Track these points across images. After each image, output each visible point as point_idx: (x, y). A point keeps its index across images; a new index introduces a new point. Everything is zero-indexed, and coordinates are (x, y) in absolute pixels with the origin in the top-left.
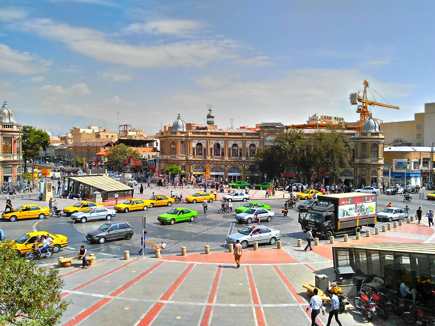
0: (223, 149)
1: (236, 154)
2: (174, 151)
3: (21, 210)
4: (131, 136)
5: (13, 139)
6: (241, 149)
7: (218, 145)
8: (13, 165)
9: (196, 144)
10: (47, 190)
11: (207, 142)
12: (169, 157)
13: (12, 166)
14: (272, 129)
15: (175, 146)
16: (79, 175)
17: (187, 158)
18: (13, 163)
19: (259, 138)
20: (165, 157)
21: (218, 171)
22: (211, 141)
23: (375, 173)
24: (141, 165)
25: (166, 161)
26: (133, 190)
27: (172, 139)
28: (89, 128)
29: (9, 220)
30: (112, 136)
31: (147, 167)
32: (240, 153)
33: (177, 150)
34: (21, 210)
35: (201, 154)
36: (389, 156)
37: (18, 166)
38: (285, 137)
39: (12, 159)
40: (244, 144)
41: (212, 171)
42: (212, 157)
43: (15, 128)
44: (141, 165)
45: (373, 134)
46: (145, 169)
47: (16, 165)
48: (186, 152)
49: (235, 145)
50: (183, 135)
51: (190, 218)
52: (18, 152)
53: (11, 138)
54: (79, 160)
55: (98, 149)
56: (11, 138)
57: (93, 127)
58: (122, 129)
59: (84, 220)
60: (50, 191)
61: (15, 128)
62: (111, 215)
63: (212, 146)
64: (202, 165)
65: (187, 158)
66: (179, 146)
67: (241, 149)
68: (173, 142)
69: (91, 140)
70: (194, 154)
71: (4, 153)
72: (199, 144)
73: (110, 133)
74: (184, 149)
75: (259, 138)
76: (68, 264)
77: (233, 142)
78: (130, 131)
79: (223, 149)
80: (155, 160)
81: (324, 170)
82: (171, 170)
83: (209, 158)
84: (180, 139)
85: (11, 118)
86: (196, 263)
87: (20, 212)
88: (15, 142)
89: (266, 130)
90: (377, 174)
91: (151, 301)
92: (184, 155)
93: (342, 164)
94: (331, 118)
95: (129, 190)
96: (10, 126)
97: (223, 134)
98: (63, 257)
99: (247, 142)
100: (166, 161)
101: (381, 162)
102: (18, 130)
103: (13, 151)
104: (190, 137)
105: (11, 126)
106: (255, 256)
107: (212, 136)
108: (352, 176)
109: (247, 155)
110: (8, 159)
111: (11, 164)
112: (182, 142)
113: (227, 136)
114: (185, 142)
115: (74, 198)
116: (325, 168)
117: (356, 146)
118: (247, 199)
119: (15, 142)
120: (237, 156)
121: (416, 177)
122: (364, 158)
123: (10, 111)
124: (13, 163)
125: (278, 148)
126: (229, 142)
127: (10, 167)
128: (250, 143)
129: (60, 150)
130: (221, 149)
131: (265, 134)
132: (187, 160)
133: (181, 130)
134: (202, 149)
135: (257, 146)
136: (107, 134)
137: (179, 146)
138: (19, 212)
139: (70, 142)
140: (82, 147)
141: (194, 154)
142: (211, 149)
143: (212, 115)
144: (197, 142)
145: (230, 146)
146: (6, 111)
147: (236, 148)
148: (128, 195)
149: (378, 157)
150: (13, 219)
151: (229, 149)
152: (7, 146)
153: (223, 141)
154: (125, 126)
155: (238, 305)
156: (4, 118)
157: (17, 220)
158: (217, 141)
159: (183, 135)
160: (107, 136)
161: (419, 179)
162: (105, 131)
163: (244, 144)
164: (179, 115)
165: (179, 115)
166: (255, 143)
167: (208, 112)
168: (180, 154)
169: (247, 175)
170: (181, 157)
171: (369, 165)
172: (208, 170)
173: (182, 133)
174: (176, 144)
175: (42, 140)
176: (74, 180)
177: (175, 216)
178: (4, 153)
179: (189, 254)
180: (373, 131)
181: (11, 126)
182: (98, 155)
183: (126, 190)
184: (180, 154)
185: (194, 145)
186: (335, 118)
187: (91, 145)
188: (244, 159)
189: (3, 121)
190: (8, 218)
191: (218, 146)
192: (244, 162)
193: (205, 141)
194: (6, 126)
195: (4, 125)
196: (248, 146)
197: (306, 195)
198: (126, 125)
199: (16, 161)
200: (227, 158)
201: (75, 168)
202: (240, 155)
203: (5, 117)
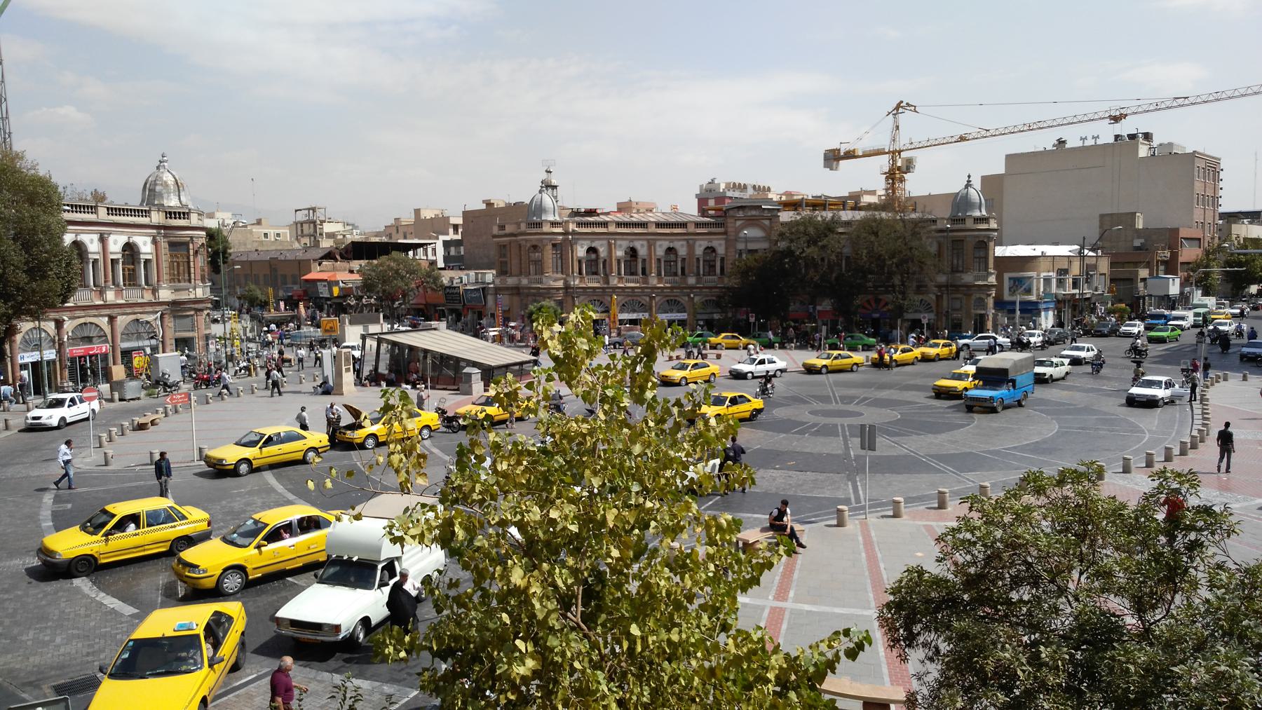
0: (644, 260)
1: (673, 270)
6: (683, 260)
7: (633, 252)
8: (197, 310)
9: (586, 248)
11: (610, 245)
12: (525, 281)
14: (754, 213)
18: (196, 306)
19: (725, 233)
20: (511, 281)
21: (634, 311)
22: (619, 242)
23: (981, 303)
24: (443, 301)
25: (516, 291)
30: (278, 235)
31: (459, 307)
32: (683, 269)
35: (596, 273)
36: (1006, 264)
38: (802, 228)
39: (192, 296)
40: (691, 248)
41: (622, 311)
42: (620, 279)
45: (978, 220)
46: (452, 311)
47: (201, 310)
48: (563, 268)
49: (670, 250)
50: (560, 230)
52: (203, 280)
53: (186, 244)
54: (258, 293)
55: (303, 266)
56: (186, 244)
57: (218, 215)
58: (301, 217)
59: (244, 468)
61: (194, 220)
63: (620, 253)
64: (599, 298)
65: (566, 282)
66: (549, 255)
67: (683, 260)
68: (535, 247)
70: (580, 273)
72: (591, 250)
73: (272, 227)
75: (725, 233)
77: (666, 244)
79: (644, 260)
80: (483, 289)
81: (868, 302)
83: (614, 282)
85: (182, 194)
88: (196, 253)
89: (741, 214)
90: (985, 307)
92: (560, 275)
93: (920, 289)
94: (745, 187)
97: (683, 225)
99: (698, 243)
101: (992, 280)
105: (185, 215)
107: (699, 231)
108: (106, 341)
109: (698, 274)
110: (183, 296)
111: (191, 309)
112: (554, 245)
113: (653, 229)
114: (562, 248)
116: (870, 297)
117: (940, 245)
118: (782, 371)
119: (196, 253)
120: (676, 274)
121: (1047, 309)
122: (958, 271)
124: (196, 306)
125: (789, 253)
126: (658, 243)
128: (705, 244)
130: (640, 261)
131: (739, 223)
132: (567, 287)
133: (551, 218)
134: (676, 261)
135: (721, 250)
137: (549, 255)
141: (580, 273)
142: (619, 262)
143: (554, 182)
144: (625, 244)
145: (660, 251)
146: (168, 178)
147: (672, 257)
149: (987, 268)
150: (371, 442)
151: (659, 260)
153: (645, 243)
158: (632, 241)
160: (266, 235)
161: (1051, 313)
162: (259, 222)
163: (691, 248)
166: (715, 244)
167: (544, 176)
169: (699, 317)
170: (555, 281)
171: (969, 287)
172: (615, 309)
173: (554, 224)
174: (542, 252)
176: (394, 344)
177: (249, 453)
180: (977, 214)
182: (307, 281)
185: (581, 251)
186: (754, 187)
187: (254, 257)
188: (692, 281)
189: (166, 203)
191: (633, 252)
192: (692, 288)
193: (605, 242)
196: (699, 251)
197: (825, 362)
198: (314, 210)
200: (653, 281)
202: (683, 273)
203: (169, 193)
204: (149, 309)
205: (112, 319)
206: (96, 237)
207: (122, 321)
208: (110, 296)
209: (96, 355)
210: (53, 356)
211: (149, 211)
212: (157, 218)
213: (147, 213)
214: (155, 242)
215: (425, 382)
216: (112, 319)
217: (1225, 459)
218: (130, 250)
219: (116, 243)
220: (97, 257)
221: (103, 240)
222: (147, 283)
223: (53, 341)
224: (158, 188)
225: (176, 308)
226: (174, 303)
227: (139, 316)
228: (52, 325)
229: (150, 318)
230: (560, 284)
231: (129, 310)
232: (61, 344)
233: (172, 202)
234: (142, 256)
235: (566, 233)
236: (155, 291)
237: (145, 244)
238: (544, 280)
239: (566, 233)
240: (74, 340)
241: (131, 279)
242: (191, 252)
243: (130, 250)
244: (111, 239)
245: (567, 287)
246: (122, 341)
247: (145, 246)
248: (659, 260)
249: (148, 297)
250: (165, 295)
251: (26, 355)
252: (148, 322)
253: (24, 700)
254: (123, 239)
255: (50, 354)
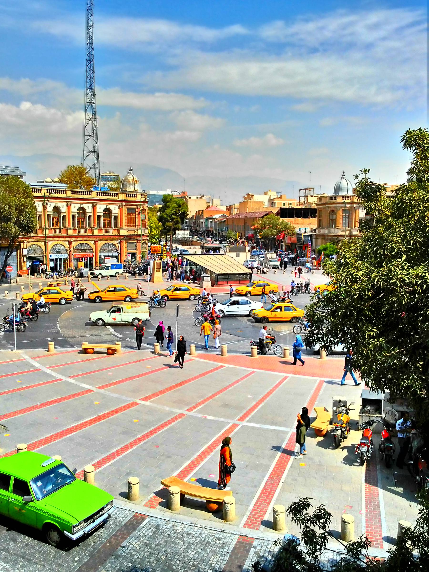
2: (333, 222)
3: (106, 291)
4: (311, 204)
5: (137, 210)
8: (138, 240)
10: (155, 270)
13: (136, 241)
15: (331, 218)
16: (221, 253)
17: (350, 232)
18: (138, 238)
24: (296, 241)
25: (324, 237)
26: (251, 274)
27: (330, 207)
28: (266, 194)
29: (94, 301)
30: (291, 204)
33: (337, 222)
34: (106, 291)
37: (143, 241)
39: (136, 233)
43: (139, 197)
44: (296, 241)
50: (348, 201)
51: (188, 296)
53: (135, 209)
57: (269, 193)
58: (302, 193)
60: (159, 271)
62: (66, 299)
65: (350, 232)
68: (333, 211)
69: (259, 209)
71: (128, 226)
73: (287, 199)
74: (347, 220)
76: (89, 351)
78: (312, 196)
82: (325, 249)
84: (342, 207)
85: (136, 185)
86: (227, 365)
87: (106, 292)
91: (124, 398)
95: (246, 274)
96: (134, 195)
98: (87, 343)
100: (323, 237)
102: (143, 199)
103: (137, 224)
104: (356, 203)
106: (321, 366)
110: (132, 233)
115: (185, 281)
123: (134, 177)
124: (138, 238)
127: (134, 243)
129: (220, 223)
132: (351, 236)
133: (344, 193)
136: (284, 202)
137: (340, 216)
138: (104, 293)
139: (235, 211)
140: (239, 219)
146: (130, 178)
148: (245, 280)
150: (98, 300)
152: (131, 218)
154: (305, 189)
155: (216, 419)
156: (128, 186)
157: (102, 301)
159: (348, 201)
164: (344, 173)
165: (344, 173)
168: (340, 227)
173: (344, 197)
174: (336, 214)
175: (179, 211)
178: (128, 226)
179: (230, 354)
181: (135, 195)
183: (243, 274)
184: (340, 227)
187: (249, 216)
189: (128, 190)
190: (93, 298)
194: (130, 194)
195: (128, 194)
198: (307, 189)
199: (139, 236)
201: (216, 244)
204: (114, 238)
205: (95, 242)
206: (65, 204)
207: (100, 244)
208: (96, 232)
209: (87, 258)
210: (66, 257)
211: (118, 194)
212: (122, 197)
213: (117, 195)
214: (119, 208)
215: (180, 278)
216: (95, 242)
217: (203, 330)
218: (107, 211)
219: (100, 208)
220: (65, 214)
221: (68, 206)
222: (64, 226)
223: (67, 250)
224: (125, 183)
225: (128, 238)
226: (127, 236)
227: (109, 242)
228: (67, 243)
229: (115, 242)
230: (347, 233)
231: (104, 239)
232: (70, 252)
233: (131, 189)
234: (87, 214)
235: (352, 203)
236: (118, 231)
237: (115, 209)
238: (336, 231)
239: (352, 203)
240: (76, 250)
241: (108, 225)
242: (137, 213)
243: (107, 211)
244: (98, 206)
245: (351, 236)
246: (101, 252)
247: (115, 209)
248: (73, 216)
249: (115, 233)
250: (124, 232)
251: (53, 255)
252: (113, 245)
253: (125, 401)
254: (104, 207)
255: (65, 256)
